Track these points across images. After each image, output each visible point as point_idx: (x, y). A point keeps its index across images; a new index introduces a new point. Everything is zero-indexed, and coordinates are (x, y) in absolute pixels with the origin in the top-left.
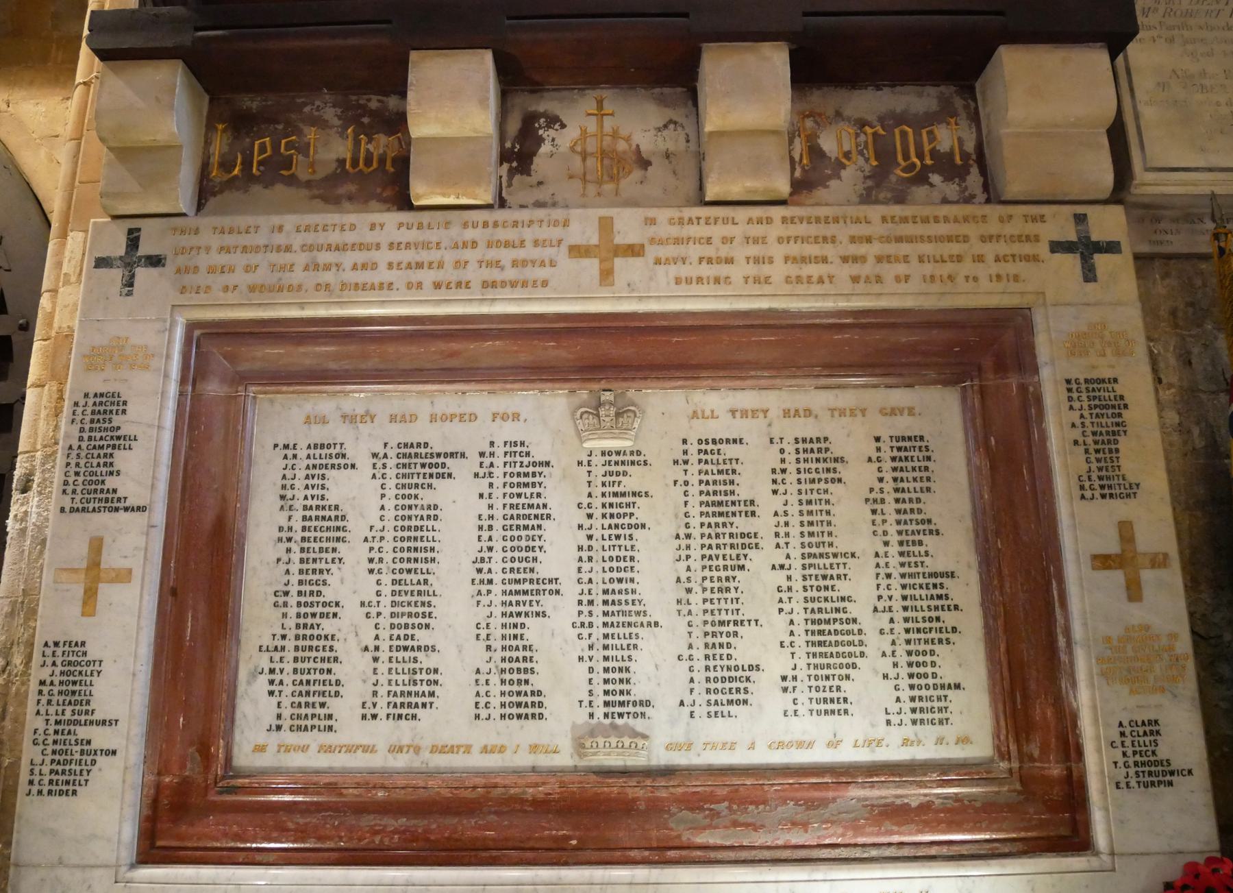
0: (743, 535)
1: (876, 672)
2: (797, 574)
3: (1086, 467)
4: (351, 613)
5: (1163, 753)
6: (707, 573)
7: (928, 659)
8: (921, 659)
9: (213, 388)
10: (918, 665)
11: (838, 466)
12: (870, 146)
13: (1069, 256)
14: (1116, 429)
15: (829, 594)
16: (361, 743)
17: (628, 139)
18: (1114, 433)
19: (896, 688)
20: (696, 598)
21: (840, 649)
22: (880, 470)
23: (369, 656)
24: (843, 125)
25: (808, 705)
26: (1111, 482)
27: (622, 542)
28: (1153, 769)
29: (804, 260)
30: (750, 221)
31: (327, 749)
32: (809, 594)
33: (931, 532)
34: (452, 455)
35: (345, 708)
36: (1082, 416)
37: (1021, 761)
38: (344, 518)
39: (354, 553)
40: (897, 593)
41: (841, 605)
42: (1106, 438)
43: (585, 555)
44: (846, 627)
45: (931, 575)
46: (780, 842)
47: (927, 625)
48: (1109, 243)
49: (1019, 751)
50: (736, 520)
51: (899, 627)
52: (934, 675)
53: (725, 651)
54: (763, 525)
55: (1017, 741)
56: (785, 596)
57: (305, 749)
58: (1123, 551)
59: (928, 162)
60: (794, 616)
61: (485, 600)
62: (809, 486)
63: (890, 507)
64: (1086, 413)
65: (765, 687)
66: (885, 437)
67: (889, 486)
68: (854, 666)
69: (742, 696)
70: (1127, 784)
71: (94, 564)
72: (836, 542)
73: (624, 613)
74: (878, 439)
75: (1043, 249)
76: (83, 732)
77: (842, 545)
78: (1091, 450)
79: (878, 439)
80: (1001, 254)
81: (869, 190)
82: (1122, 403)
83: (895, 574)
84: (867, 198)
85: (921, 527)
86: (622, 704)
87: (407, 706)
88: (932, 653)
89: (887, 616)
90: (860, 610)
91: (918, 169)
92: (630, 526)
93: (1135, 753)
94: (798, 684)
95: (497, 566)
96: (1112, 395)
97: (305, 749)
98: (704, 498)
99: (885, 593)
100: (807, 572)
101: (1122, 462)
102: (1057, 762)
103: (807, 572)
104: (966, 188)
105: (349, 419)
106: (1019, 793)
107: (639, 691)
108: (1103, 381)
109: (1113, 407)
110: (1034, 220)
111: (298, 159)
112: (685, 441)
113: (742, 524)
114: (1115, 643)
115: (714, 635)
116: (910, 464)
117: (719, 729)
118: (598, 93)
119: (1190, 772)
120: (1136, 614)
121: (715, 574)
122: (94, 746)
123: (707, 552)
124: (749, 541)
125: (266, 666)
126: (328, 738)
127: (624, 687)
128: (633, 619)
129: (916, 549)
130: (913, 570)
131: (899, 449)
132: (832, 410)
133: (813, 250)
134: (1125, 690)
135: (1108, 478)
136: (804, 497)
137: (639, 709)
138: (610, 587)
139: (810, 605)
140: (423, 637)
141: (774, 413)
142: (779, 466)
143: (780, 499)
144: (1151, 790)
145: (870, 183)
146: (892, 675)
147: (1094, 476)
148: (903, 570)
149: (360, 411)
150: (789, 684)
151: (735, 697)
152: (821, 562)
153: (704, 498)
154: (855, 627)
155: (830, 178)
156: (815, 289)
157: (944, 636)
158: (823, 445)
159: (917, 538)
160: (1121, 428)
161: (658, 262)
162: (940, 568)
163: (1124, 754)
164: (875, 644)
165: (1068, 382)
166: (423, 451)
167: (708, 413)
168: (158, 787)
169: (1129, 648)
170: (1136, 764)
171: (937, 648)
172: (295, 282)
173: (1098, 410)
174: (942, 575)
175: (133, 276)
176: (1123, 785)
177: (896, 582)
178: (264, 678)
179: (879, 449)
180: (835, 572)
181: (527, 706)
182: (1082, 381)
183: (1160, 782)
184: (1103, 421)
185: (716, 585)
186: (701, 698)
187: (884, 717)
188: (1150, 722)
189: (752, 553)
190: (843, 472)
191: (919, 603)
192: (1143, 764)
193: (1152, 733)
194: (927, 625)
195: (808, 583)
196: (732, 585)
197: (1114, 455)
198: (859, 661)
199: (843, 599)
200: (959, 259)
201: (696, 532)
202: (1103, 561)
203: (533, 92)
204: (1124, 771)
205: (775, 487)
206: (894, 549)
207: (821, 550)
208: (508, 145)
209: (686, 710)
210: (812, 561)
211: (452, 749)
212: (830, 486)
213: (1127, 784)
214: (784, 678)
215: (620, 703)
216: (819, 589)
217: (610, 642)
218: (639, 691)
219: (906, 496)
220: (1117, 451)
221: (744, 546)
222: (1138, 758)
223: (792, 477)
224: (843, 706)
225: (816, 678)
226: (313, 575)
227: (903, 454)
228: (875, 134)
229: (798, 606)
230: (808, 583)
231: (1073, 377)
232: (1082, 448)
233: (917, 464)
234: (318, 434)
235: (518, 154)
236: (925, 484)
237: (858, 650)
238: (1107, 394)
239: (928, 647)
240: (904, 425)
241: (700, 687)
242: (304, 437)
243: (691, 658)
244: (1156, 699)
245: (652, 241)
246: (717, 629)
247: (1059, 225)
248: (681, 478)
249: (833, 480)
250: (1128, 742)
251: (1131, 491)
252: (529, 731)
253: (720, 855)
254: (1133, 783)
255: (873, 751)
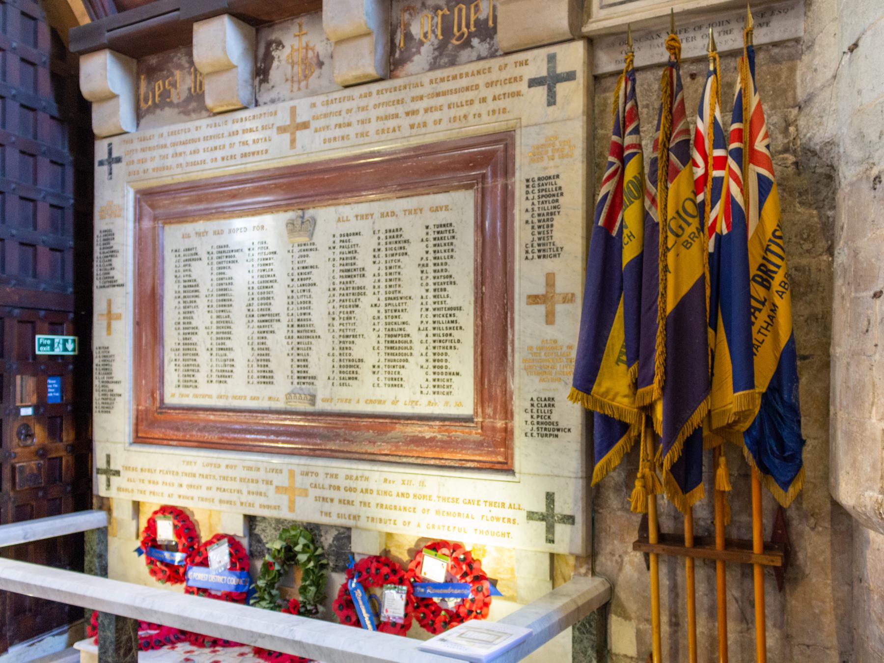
0: (359, 288)
1: (417, 364)
2: (382, 309)
3: (531, 238)
4: (202, 332)
5: (554, 418)
6: (342, 309)
7: (444, 357)
8: (440, 357)
9: (147, 224)
10: (438, 361)
11: (406, 245)
12: (439, 25)
13: (541, 88)
14: (553, 211)
15: (397, 320)
16: (206, 393)
17: (313, 49)
18: (551, 214)
19: (427, 374)
20: (336, 323)
21: (401, 351)
22: (427, 246)
23: (209, 352)
24: (426, 12)
25: (384, 382)
26: (545, 247)
27: (306, 293)
28: (548, 426)
29: (387, 118)
30: (361, 96)
31: (196, 396)
32: (387, 320)
33: (451, 283)
34: (237, 251)
35: (201, 377)
36: (533, 204)
37: (484, 418)
38: (198, 286)
39: (202, 302)
40: (431, 319)
41: (402, 326)
42: (545, 218)
43: (290, 301)
44: (404, 339)
45: (449, 309)
46: (363, 451)
47: (445, 338)
48: (567, 73)
49: (483, 412)
50: (355, 279)
51: (431, 339)
52: (446, 367)
53: (348, 351)
54: (368, 282)
55: (482, 406)
56: (376, 321)
57: (187, 396)
58: (547, 292)
59: (473, 29)
60: (380, 333)
61: (251, 325)
62: (391, 258)
63: (431, 268)
64: (536, 202)
65: (365, 371)
66: (431, 226)
67: (431, 256)
68: (407, 361)
69: (355, 376)
70: (532, 435)
71: (109, 312)
72: (402, 290)
73: (306, 331)
74: (427, 227)
75: (523, 86)
76: (111, 386)
77: (405, 292)
78: (536, 227)
79: (427, 227)
80: (497, 94)
81: (435, 58)
82: (559, 192)
83: (431, 309)
84: (434, 66)
85: (446, 280)
86: (304, 378)
87: (224, 376)
88: (446, 354)
89: (425, 333)
90: (411, 329)
91: (466, 36)
92: (309, 285)
93: (538, 416)
94: (380, 369)
95: (255, 307)
96: (554, 187)
97: (187, 396)
98: (342, 268)
99: (425, 320)
100: (387, 308)
101: (555, 234)
102: (500, 419)
103: (387, 308)
104: (493, 45)
105: (198, 234)
106: (482, 435)
107: (312, 371)
108: (550, 178)
109: (554, 195)
110: (521, 64)
111: (173, 91)
112: (334, 236)
113: (358, 282)
114: (535, 350)
115: (344, 342)
116: (443, 242)
117: (345, 392)
118: (297, 21)
119: (569, 430)
120: (550, 332)
121: (345, 310)
122: (115, 392)
123: (342, 298)
124: (361, 291)
125: (174, 357)
126: (195, 391)
127: (305, 369)
128: (310, 334)
129: (442, 293)
130: (440, 306)
131: (438, 232)
132: (405, 211)
133: (391, 110)
134: (536, 379)
135: (544, 245)
136: (388, 265)
137: (311, 381)
138: (300, 317)
139: (388, 327)
140: (228, 344)
141: (377, 215)
142: (377, 247)
143: (377, 266)
144: (545, 439)
145: (437, 53)
146: (425, 366)
147: (535, 244)
148: (435, 306)
149: (202, 230)
150: (376, 370)
151: (351, 376)
152: (394, 302)
153: (342, 268)
154: (408, 339)
155: (414, 54)
156: (391, 135)
157: (453, 345)
158: (399, 233)
159: (443, 287)
160: (557, 210)
161: (316, 131)
162: (454, 305)
163: (532, 417)
164: (418, 348)
165: (528, 181)
166: (226, 249)
167: (345, 218)
168: (138, 410)
169: (543, 354)
170: (538, 423)
171: (449, 351)
172: (169, 165)
173: (544, 199)
174: (455, 309)
175: (111, 169)
176: (529, 434)
177: (430, 313)
178: (173, 363)
179: (427, 234)
180: (400, 308)
181: (267, 378)
182: (536, 179)
183: (550, 435)
184: (546, 206)
185: (346, 316)
186: (337, 376)
187: (419, 390)
188: (549, 399)
189: (362, 298)
190: (409, 249)
191: (441, 325)
192: (542, 423)
193: (549, 405)
194: (445, 338)
195: (387, 314)
196: (352, 315)
197: (550, 229)
198: (409, 358)
199: (404, 323)
200: (471, 102)
201: (337, 287)
202: (534, 299)
203: (269, 26)
204: (531, 426)
205: (374, 260)
206: (431, 294)
207: (395, 295)
208: (259, 65)
209: (331, 382)
210: (391, 302)
211: (240, 398)
212: (401, 258)
213: (532, 435)
214: (374, 367)
215: (304, 377)
216: (392, 317)
217: (300, 346)
218: (312, 371)
219: (440, 261)
220: (552, 226)
221: (359, 294)
222: (539, 419)
223: (382, 253)
224: (400, 383)
225: (389, 367)
226: (188, 314)
227: (440, 236)
228: (443, 16)
229: (382, 327)
230: (387, 314)
231: (530, 177)
232: (530, 226)
233: (447, 241)
234: (188, 244)
235: (261, 72)
236: (451, 254)
237: (408, 352)
238: (550, 187)
239: (444, 351)
240: (442, 217)
241: (337, 370)
242: (183, 244)
243: (333, 355)
244: (554, 385)
245: (314, 118)
246: (345, 339)
247: (536, 64)
248: (332, 257)
249: (403, 254)
250: (535, 410)
251: (557, 252)
252: (268, 390)
253: (337, 454)
254: (535, 434)
255: (413, 408)
